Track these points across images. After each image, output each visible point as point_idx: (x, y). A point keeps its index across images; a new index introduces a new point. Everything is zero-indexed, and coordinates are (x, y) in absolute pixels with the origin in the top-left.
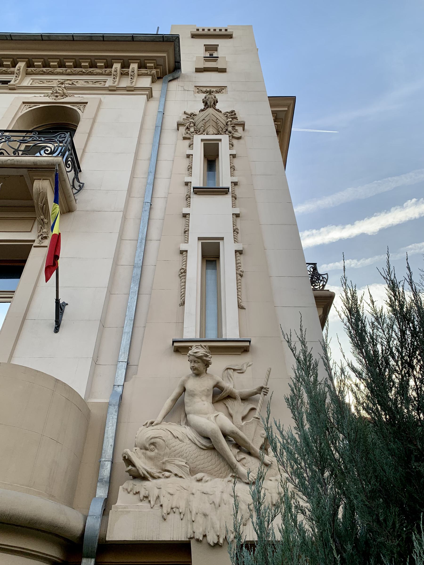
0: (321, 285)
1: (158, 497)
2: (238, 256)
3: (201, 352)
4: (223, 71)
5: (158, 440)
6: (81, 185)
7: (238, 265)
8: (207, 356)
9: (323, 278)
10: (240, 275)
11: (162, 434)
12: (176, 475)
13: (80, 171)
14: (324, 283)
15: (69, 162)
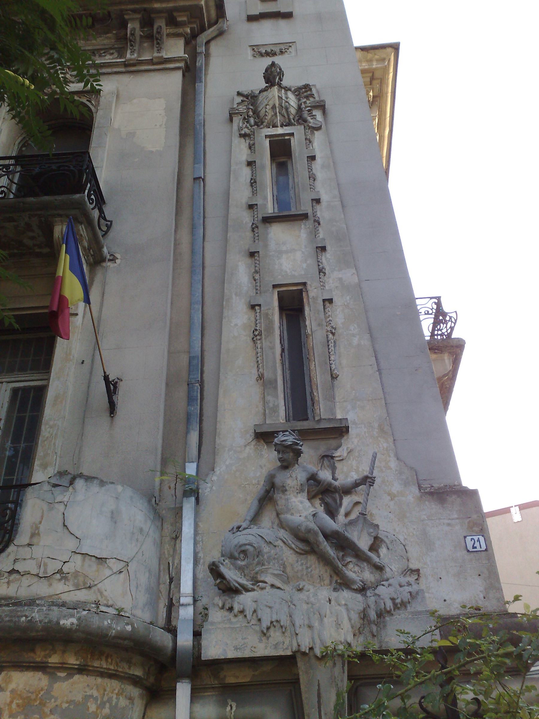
0: (448, 327)
1: (255, 611)
2: (329, 307)
3: (290, 439)
4: (288, 16)
5: (248, 547)
6: (109, 223)
7: (328, 320)
8: (297, 444)
9: (450, 317)
10: (332, 333)
11: (251, 539)
12: (272, 586)
13: (104, 203)
14: (453, 325)
15: (93, 197)
